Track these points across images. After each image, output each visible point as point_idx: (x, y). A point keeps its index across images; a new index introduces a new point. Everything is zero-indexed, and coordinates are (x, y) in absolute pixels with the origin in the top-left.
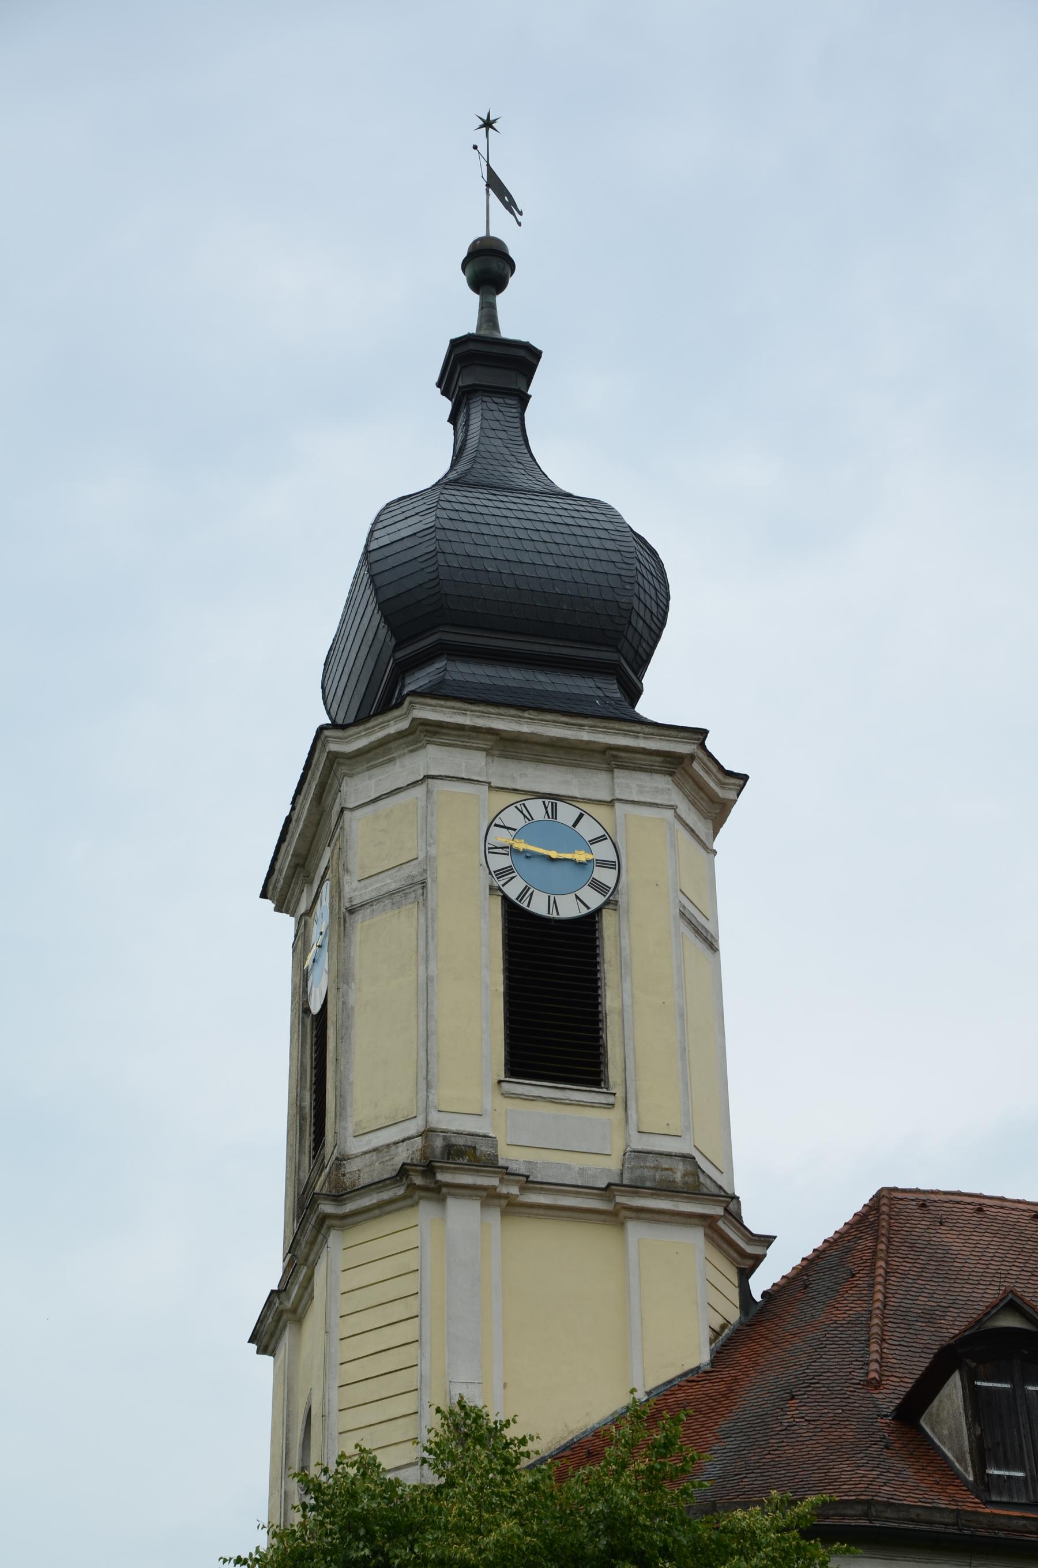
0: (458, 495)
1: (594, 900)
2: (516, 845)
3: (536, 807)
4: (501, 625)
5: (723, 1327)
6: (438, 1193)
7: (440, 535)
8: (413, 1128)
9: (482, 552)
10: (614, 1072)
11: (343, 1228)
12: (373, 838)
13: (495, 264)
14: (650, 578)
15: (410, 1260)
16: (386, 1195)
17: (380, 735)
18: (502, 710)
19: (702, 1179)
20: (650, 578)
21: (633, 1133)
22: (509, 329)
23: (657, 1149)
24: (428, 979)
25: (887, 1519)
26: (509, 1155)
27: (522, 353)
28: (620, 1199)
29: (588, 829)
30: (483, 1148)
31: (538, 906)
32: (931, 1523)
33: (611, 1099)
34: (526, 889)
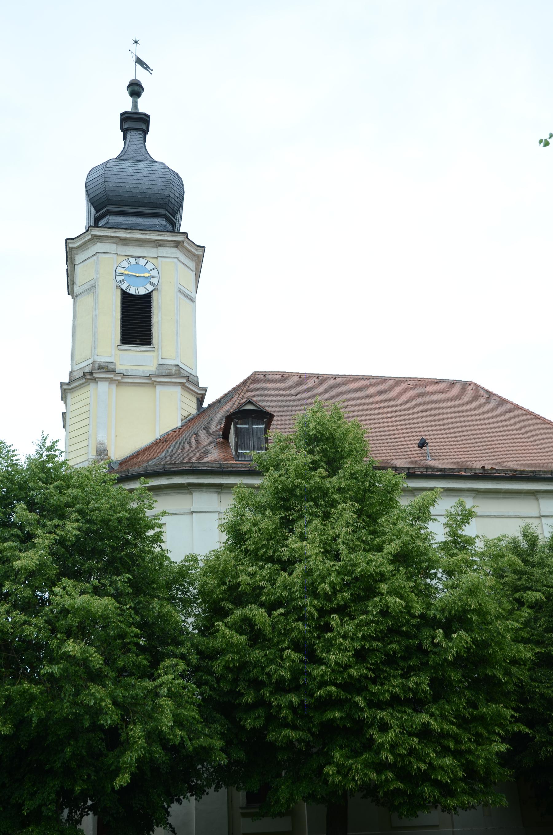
0: (121, 163)
1: (150, 288)
2: (125, 273)
3: (133, 261)
4: (135, 204)
5: (189, 416)
6: (95, 380)
7: (106, 176)
8: (90, 361)
9: (119, 180)
10: (155, 340)
11: (71, 392)
12: (83, 274)
13: (136, 88)
14: (176, 186)
15: (87, 401)
16: (81, 382)
17: (84, 240)
18: (120, 230)
19: (182, 371)
20: (176, 186)
21: (160, 359)
22: (142, 109)
23: (167, 363)
24: (96, 316)
25: (198, 467)
26: (120, 368)
27: (143, 116)
28: (153, 379)
29: (149, 266)
30: (111, 366)
31: (132, 291)
32: (213, 467)
33: (153, 349)
34: (128, 286)
